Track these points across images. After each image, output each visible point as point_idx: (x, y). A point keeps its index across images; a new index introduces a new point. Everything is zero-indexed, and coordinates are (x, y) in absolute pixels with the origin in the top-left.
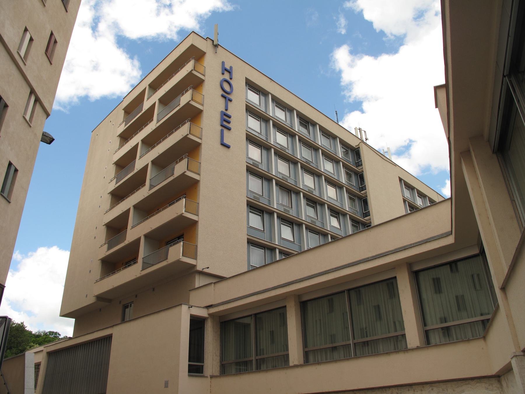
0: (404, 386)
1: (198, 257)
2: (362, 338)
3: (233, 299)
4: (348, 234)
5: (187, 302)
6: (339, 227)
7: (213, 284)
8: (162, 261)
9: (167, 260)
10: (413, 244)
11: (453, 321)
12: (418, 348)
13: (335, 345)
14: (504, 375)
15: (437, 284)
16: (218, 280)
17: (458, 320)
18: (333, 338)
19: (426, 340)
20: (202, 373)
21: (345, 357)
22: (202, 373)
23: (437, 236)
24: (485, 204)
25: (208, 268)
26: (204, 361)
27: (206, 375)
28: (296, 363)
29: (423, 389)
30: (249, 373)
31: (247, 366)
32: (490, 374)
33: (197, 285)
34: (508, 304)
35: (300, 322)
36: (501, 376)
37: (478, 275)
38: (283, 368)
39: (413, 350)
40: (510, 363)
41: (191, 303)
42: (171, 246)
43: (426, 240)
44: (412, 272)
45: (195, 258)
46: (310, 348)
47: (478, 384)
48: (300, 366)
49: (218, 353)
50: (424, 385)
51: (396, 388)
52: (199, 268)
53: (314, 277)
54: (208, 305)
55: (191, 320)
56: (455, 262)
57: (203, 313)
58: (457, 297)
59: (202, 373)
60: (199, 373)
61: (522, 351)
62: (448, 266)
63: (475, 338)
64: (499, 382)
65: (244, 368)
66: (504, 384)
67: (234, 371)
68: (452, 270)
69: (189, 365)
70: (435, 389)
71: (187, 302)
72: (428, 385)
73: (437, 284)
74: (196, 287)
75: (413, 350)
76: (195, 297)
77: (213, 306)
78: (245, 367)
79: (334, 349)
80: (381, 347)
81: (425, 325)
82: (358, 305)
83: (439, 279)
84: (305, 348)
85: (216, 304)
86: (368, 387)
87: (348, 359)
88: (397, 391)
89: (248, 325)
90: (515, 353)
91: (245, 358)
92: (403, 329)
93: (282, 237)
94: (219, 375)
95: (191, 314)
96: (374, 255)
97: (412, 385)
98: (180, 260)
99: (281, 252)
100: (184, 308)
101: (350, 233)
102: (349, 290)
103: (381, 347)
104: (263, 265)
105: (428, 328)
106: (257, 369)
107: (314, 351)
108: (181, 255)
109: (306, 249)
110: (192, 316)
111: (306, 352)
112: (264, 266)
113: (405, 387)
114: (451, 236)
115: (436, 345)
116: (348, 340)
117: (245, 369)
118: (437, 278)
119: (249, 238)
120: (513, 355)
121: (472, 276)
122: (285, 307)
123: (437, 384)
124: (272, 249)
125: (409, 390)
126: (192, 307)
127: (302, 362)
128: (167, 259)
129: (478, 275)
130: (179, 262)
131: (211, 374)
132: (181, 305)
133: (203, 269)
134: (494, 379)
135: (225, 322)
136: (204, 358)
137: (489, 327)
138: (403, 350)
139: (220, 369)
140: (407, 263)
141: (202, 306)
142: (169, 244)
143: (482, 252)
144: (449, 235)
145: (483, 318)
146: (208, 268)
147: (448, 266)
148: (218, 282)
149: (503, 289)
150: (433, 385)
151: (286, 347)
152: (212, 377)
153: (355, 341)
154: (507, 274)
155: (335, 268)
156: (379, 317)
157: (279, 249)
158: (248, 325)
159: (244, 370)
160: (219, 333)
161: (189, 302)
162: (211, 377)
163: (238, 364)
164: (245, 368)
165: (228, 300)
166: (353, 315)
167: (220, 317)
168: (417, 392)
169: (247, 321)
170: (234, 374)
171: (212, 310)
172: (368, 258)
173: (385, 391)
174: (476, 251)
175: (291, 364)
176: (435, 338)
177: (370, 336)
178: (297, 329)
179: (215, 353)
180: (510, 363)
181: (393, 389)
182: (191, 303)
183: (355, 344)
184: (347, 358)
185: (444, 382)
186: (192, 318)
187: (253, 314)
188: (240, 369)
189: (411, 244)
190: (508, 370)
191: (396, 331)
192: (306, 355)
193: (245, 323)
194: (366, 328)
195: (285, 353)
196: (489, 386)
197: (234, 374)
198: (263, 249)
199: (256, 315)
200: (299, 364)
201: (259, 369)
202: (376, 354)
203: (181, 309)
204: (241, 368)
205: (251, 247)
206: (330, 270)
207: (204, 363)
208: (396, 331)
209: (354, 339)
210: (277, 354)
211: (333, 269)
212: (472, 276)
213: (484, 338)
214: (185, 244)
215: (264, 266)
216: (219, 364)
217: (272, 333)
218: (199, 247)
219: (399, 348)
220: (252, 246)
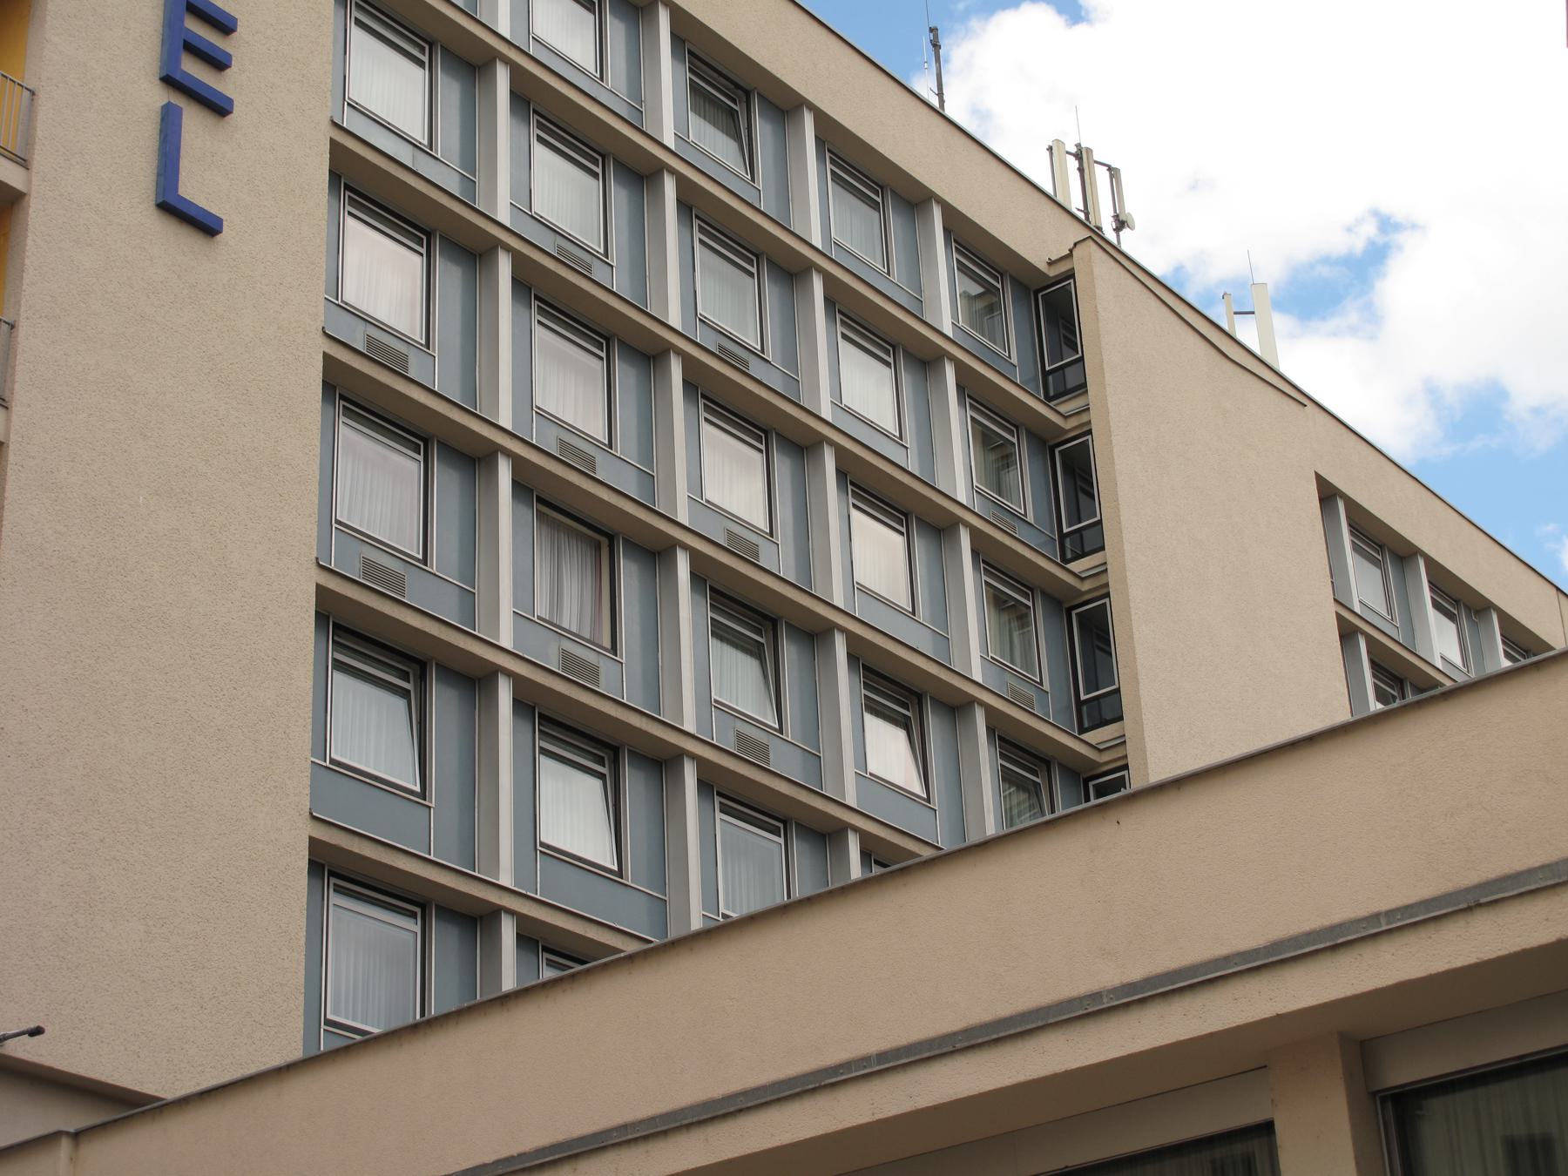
4: (974, 838)
6: (917, 787)
7: (65, 1145)
10: (1390, 914)
23: (1542, 868)
25: (37, 1032)
43: (1468, 890)
44: (1374, 1094)
53: (740, 1111)
93: (546, 836)
96: (1135, 974)
99: (533, 939)
101: (991, 830)
104: (410, 1021)
109: (696, 924)
112: (414, 1029)
146: (37, 1032)
148: (103, 1126)
155: (882, 1056)
157: (522, 921)
189: (1375, 917)
198: (413, 915)
211: (865, 1060)
215: (414, 1029)
220: (339, 890)
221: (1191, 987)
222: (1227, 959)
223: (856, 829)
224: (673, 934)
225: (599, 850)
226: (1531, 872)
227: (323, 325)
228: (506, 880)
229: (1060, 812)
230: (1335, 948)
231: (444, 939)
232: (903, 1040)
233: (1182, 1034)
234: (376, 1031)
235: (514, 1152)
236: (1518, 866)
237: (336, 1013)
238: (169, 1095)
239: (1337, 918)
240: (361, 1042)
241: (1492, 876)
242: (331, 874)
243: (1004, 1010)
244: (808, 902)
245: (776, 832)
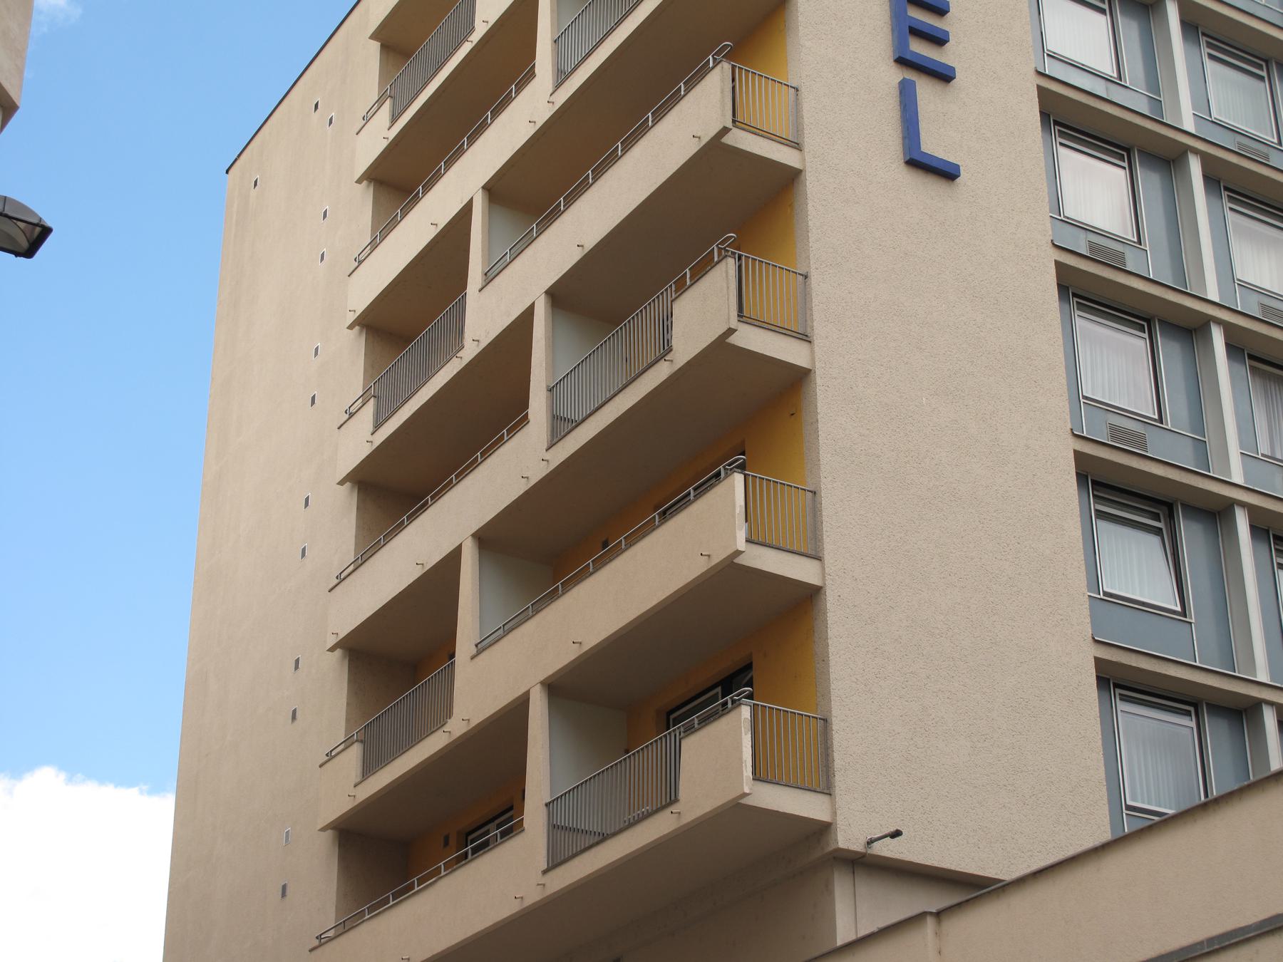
1: (840, 781)
7: (930, 923)
9: (675, 808)
25: (896, 834)
42: (690, 730)
45: (827, 789)
52: (849, 838)
74: (839, 943)
104: (1197, 802)
108: (748, 771)
130: (737, 811)
133: (870, 842)
142: (677, 721)
146: (896, 834)
148: (959, 905)
198: (1188, 713)
205: (1122, 706)
218: (836, 725)
220: (1124, 698)
228: (1263, 677)
231: (1217, 731)
234: (1171, 812)
237: (1133, 799)
238: (1008, 875)
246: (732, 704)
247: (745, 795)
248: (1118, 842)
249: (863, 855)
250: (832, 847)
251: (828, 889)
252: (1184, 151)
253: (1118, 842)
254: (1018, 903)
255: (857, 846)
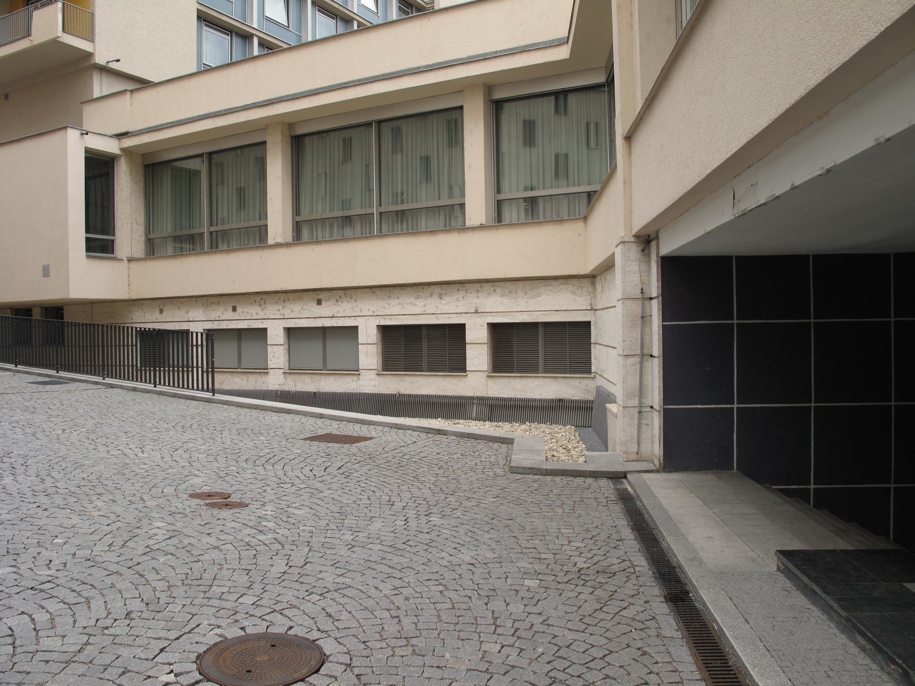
0: (451, 284)
1: (97, 38)
2: (393, 204)
3: (167, 123)
4: (389, 20)
5: (77, 124)
6: (374, 9)
7: (128, 94)
8: (19, 39)
9: (30, 38)
10: (500, 51)
11: (544, 188)
12: (481, 227)
13: (347, 213)
14: (601, 274)
15: (529, 131)
16: (140, 86)
17: (552, 188)
18: (346, 204)
19: (496, 215)
20: (113, 252)
21: (362, 235)
22: (113, 253)
23: (542, 42)
24: (632, 4)
25: (118, 61)
26: (116, 232)
27: (119, 257)
28: (280, 240)
29: (480, 289)
30: (196, 254)
31: (193, 244)
32: (582, 273)
33: (96, 94)
34: (630, 164)
35: (291, 176)
36: (598, 276)
37: (597, 124)
38: (257, 248)
39: (473, 229)
40: (613, 256)
41: (86, 127)
42: (36, 8)
43: (522, 47)
44: (490, 100)
45: (92, 40)
46: (305, 214)
47: (562, 287)
48: (287, 245)
49: (141, 219)
50: (483, 284)
51: (440, 286)
52: (100, 59)
53: (319, 93)
54: (119, 132)
55: (86, 158)
56: (565, 92)
57: (110, 147)
58: (557, 156)
59: (113, 253)
60: (107, 253)
61: (633, 236)
62: (553, 98)
63: (572, 218)
64: (593, 284)
65: (188, 247)
66: (599, 287)
67: (170, 251)
68: (557, 111)
69: (87, 239)
70: (498, 290)
71: (77, 124)
72: (489, 284)
73: (529, 131)
74: (94, 97)
75: (473, 229)
76: (93, 116)
77: (129, 135)
78: (189, 244)
79: (347, 220)
80: (423, 222)
81: (499, 191)
82: (393, 153)
83: (534, 122)
84: (297, 215)
85: (135, 132)
86: (395, 282)
87: (367, 238)
88: (439, 290)
89: (197, 173)
90: (623, 237)
91: (190, 229)
92: (463, 195)
93: (267, 14)
94: (143, 256)
95: (85, 147)
96: (430, 63)
97: (465, 283)
98: (58, 39)
99: (263, 44)
100: (72, 135)
101: (394, 18)
102: (379, 122)
103: (423, 222)
104: (227, 63)
105: (502, 197)
106: (212, 249)
107: (310, 222)
108: (60, 28)
109: (310, 39)
110: (88, 151)
111: (297, 222)
112: (228, 65)
113: (453, 285)
114: (566, 45)
115: (511, 225)
116: (370, 207)
117: (190, 248)
118: (530, 121)
119: (348, 379)
120: (620, 241)
121: (588, 124)
122: (265, 143)
123: (503, 283)
124: (246, 37)
125: (458, 290)
126: (87, 134)
127: (289, 239)
128: (29, 34)
129: (597, 124)
130: (55, 43)
131: (129, 255)
132: (65, 128)
133: (108, 62)
134: (586, 280)
135: (153, 164)
136: (116, 228)
137: (596, 201)
138: (459, 227)
139: (146, 247)
140: (484, 84)
141: (109, 134)
142: (31, 4)
143: (610, 82)
144: (563, 44)
145: (589, 189)
146: (118, 61)
147: (553, 98)
148: (139, 89)
149: (629, 138)
150: (497, 284)
151: (263, 213)
152: (130, 260)
153: (382, 209)
154: (639, 114)
155: (359, 80)
156: (427, 177)
157: (260, 38)
158: (197, 173)
159: (188, 250)
160: (142, 184)
161: (81, 124)
162: (128, 260)
163: (177, 239)
164: (191, 247)
165: (158, 124)
166: (383, 166)
167: (144, 156)
168: (471, 293)
169: (194, 165)
170: (170, 256)
171: (128, 143)
172: (419, 68)
173: (421, 290)
174: (601, 79)
175: (271, 241)
176: (509, 214)
177: (408, 203)
178: (283, 183)
179: (136, 220)
180: (613, 256)
181: (435, 287)
182: (86, 127)
183: (380, 213)
184: (367, 236)
185: (513, 281)
186: (89, 155)
187: (207, 153)
188: (181, 248)
189: (496, 52)
190: (608, 266)
191: (451, 196)
192: (297, 228)
193: (190, 169)
194: (402, 193)
195: (262, 223)
196: (578, 289)
197: (170, 256)
198: (228, 34)
199: (210, 154)
200: (284, 242)
201: (214, 247)
202: (415, 232)
203: (67, 136)
204: (184, 246)
205: (205, 28)
206: (349, 82)
207: (114, 236)
208: (451, 196)
209: (380, 206)
210: (246, 225)
211: (354, 81)
212: (588, 124)
213: (585, 219)
214: (67, 6)
215: (228, 65)
216: (143, 238)
217: (241, 191)
218: (97, 16)
219: (452, 226)
220: (206, 25)
221: (431, 70)
222: (456, 60)
223: (356, 20)
224: (303, 42)
225: (281, 18)
226: (540, 43)
227: (641, 287)
228: (255, 26)
229: (414, 14)
230: (485, 59)
231: (237, 41)
232: (365, 77)
233: (442, 80)
234: (214, 66)
235: (256, 101)
236: (536, 41)
237: (206, 61)
238: (156, 82)
239: (486, 51)
240: (209, 69)
241: (529, 43)
242: (204, 20)
243: (394, 70)
244: (341, 35)
245: (333, 19)
246: (358, 27)
247: (59, 37)
248: (198, 73)
249: (105, 67)
250: (93, 62)
251: (91, 77)
252: (353, 19)
253: (198, 73)
254: (161, 91)
255: (103, 63)
